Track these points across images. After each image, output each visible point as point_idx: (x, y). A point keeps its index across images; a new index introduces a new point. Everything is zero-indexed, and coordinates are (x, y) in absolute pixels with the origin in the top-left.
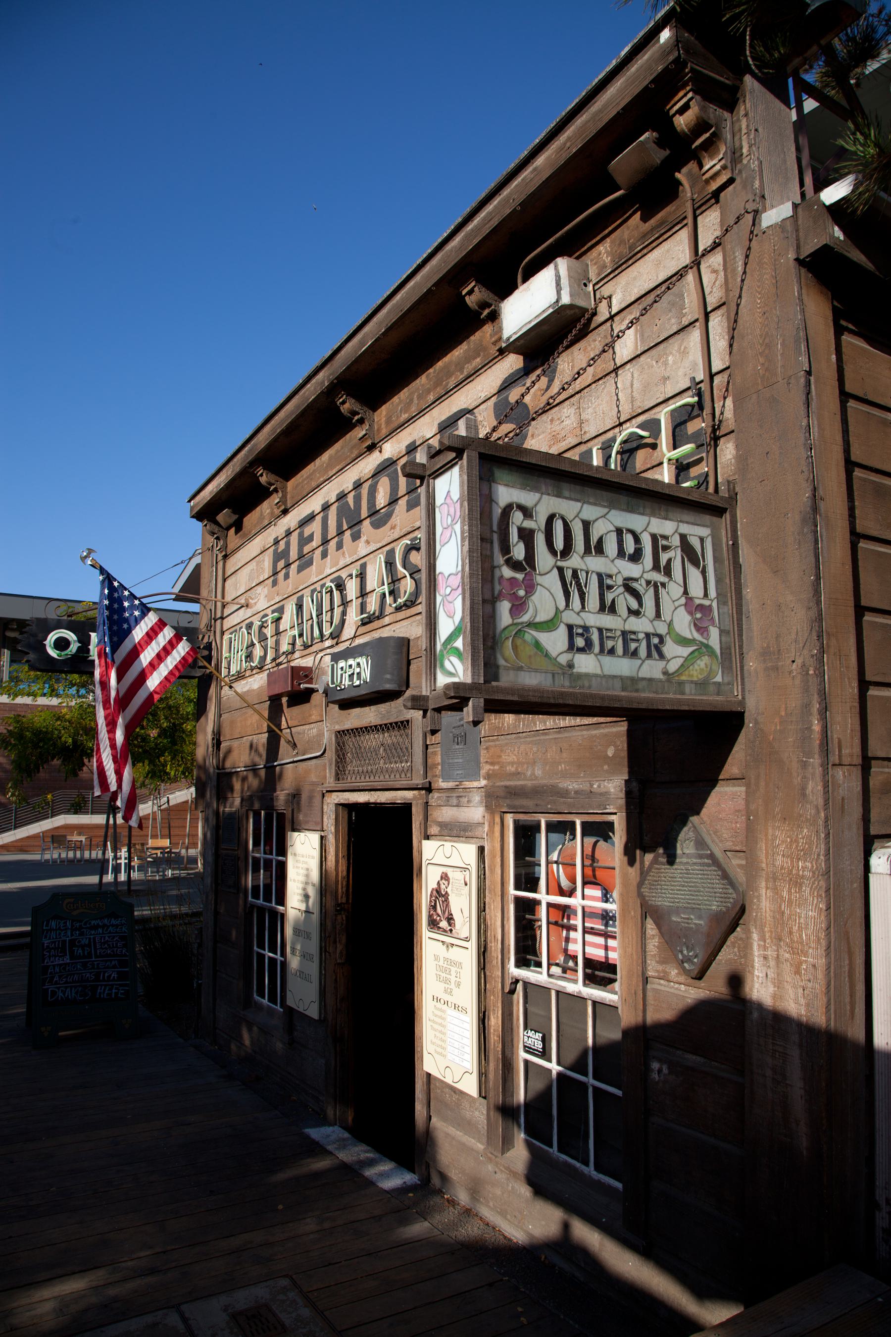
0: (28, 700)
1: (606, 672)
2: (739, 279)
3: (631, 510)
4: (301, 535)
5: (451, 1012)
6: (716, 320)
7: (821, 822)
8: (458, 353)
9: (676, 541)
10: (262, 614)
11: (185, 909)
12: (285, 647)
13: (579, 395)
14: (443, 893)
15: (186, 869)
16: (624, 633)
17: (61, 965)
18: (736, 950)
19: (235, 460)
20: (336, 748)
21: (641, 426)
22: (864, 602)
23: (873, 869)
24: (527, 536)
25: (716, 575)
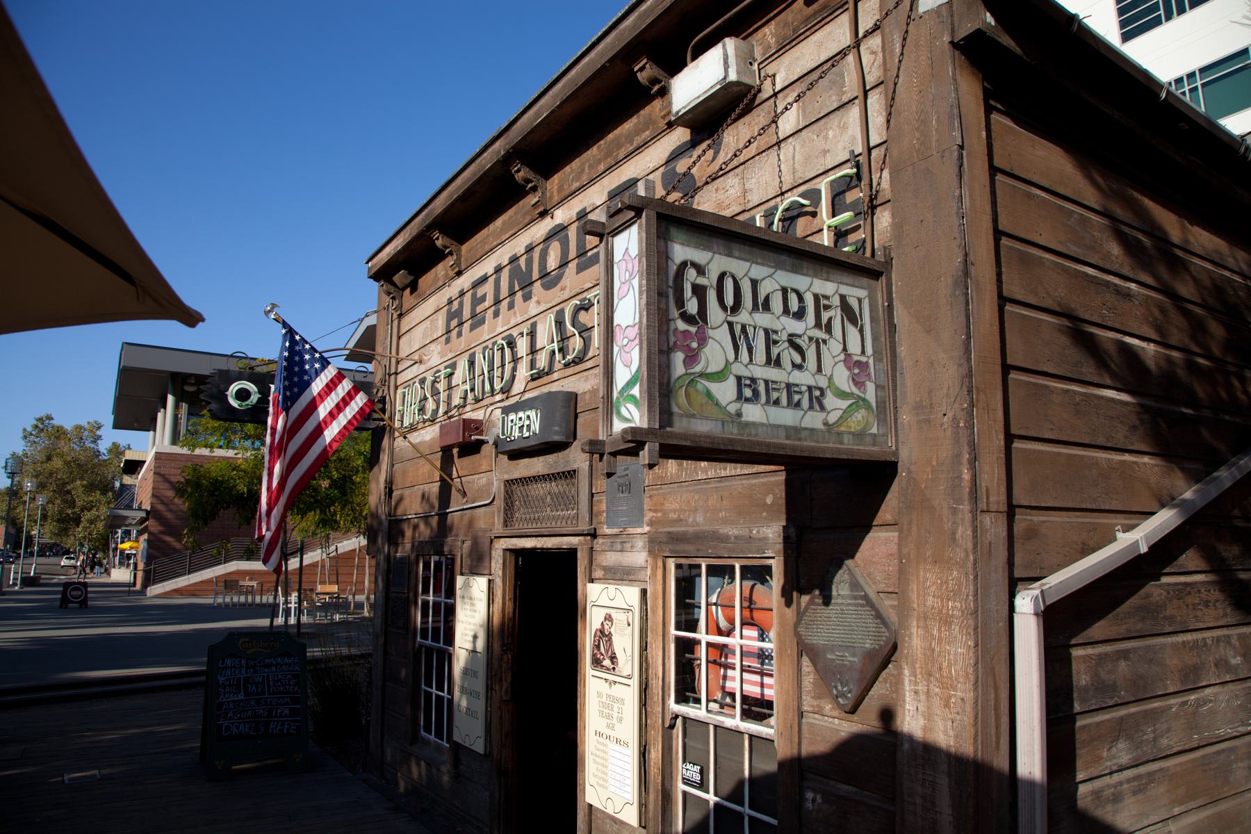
0: (205, 452)
1: (772, 421)
2: (897, 60)
3: (795, 270)
4: (474, 295)
5: (612, 746)
6: (874, 98)
7: (970, 565)
8: (628, 126)
9: (836, 301)
10: (435, 369)
11: (354, 651)
12: (456, 401)
13: (743, 166)
14: (607, 633)
15: (353, 614)
16: (789, 386)
17: (235, 701)
18: (888, 685)
19: (413, 224)
20: (505, 496)
21: (802, 195)
22: (1010, 361)
23: (1017, 610)
24: (699, 291)
25: (872, 334)
